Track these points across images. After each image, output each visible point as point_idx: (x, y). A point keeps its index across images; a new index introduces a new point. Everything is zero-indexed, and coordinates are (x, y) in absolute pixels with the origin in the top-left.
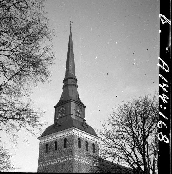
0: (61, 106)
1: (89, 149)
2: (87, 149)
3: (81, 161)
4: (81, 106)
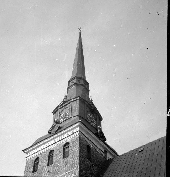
0: (64, 108)
4: (69, 103)
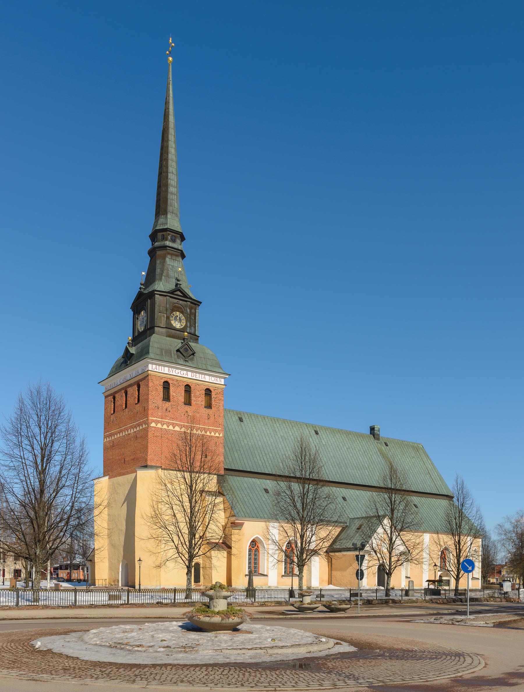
1: (193, 402)
2: (188, 402)
3: (171, 427)
